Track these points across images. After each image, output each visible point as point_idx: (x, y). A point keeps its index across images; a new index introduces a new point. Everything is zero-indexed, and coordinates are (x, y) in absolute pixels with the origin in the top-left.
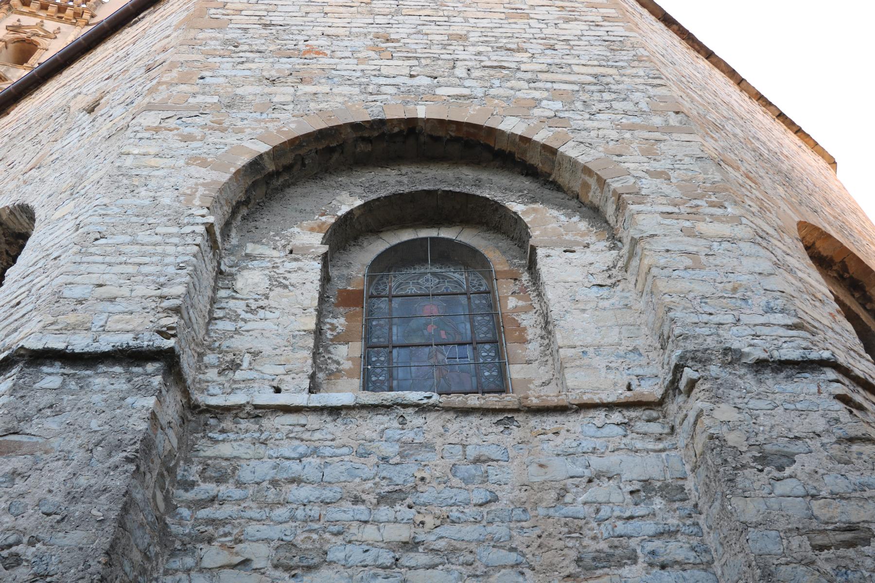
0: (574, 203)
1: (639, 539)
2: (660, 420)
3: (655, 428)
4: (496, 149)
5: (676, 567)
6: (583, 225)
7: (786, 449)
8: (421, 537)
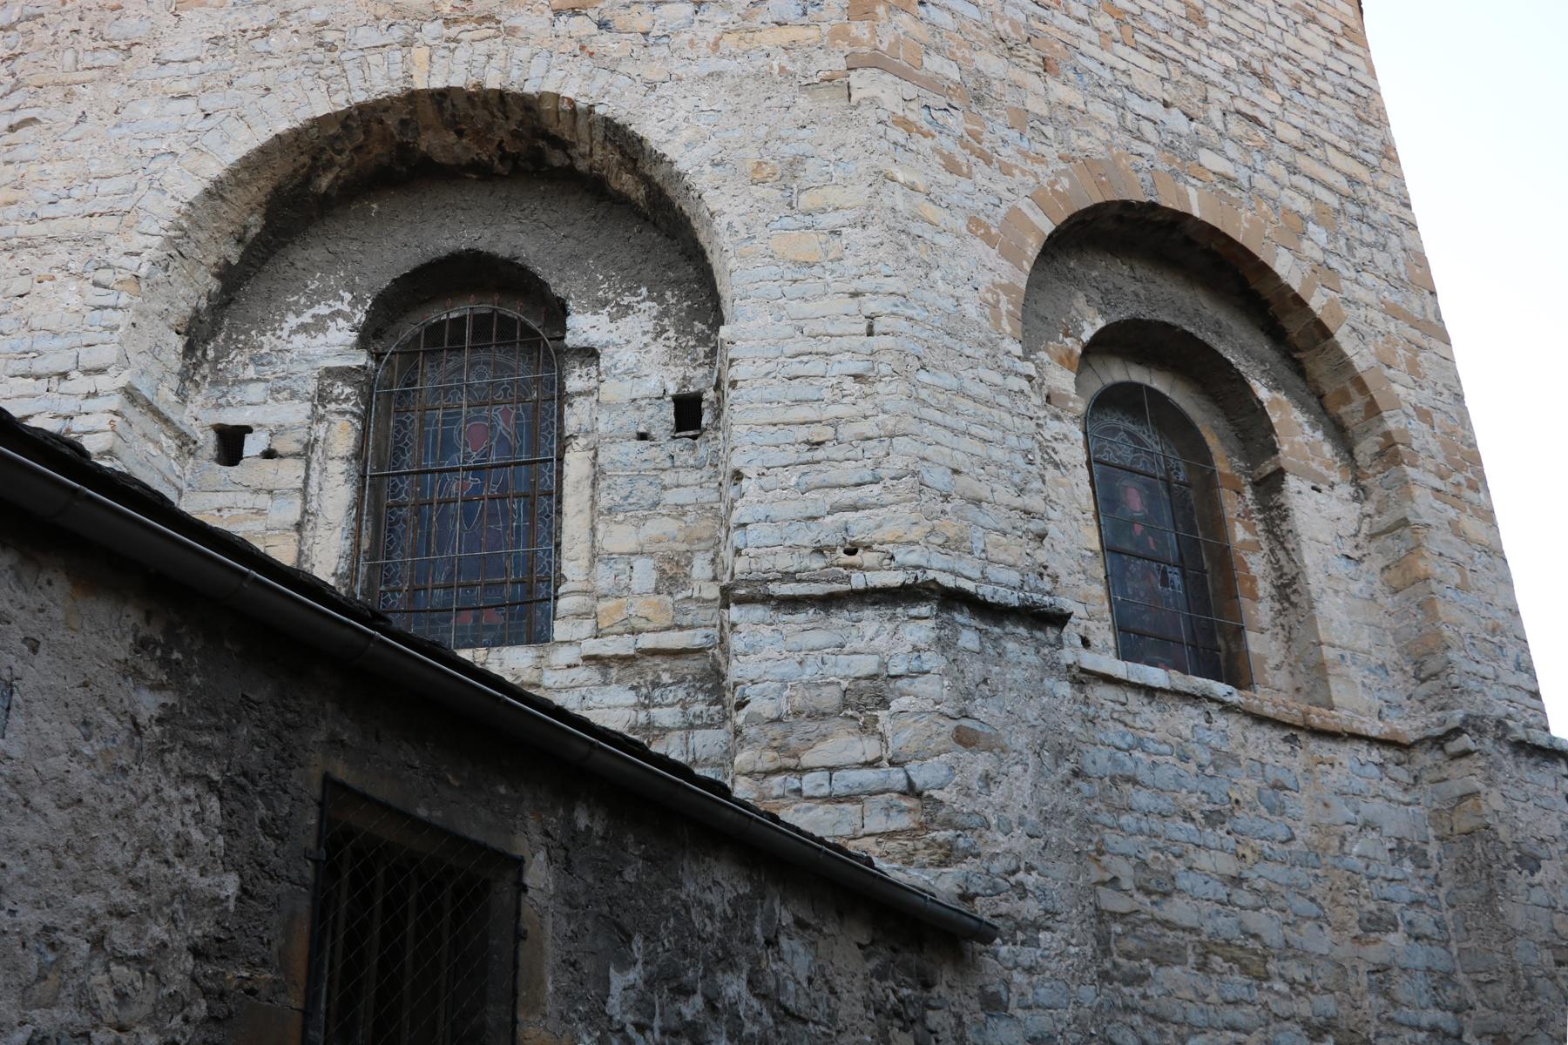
0: (1313, 401)
2: (1406, 766)
3: (1402, 774)
4: (1253, 287)
6: (1327, 449)
8: (1246, 874)
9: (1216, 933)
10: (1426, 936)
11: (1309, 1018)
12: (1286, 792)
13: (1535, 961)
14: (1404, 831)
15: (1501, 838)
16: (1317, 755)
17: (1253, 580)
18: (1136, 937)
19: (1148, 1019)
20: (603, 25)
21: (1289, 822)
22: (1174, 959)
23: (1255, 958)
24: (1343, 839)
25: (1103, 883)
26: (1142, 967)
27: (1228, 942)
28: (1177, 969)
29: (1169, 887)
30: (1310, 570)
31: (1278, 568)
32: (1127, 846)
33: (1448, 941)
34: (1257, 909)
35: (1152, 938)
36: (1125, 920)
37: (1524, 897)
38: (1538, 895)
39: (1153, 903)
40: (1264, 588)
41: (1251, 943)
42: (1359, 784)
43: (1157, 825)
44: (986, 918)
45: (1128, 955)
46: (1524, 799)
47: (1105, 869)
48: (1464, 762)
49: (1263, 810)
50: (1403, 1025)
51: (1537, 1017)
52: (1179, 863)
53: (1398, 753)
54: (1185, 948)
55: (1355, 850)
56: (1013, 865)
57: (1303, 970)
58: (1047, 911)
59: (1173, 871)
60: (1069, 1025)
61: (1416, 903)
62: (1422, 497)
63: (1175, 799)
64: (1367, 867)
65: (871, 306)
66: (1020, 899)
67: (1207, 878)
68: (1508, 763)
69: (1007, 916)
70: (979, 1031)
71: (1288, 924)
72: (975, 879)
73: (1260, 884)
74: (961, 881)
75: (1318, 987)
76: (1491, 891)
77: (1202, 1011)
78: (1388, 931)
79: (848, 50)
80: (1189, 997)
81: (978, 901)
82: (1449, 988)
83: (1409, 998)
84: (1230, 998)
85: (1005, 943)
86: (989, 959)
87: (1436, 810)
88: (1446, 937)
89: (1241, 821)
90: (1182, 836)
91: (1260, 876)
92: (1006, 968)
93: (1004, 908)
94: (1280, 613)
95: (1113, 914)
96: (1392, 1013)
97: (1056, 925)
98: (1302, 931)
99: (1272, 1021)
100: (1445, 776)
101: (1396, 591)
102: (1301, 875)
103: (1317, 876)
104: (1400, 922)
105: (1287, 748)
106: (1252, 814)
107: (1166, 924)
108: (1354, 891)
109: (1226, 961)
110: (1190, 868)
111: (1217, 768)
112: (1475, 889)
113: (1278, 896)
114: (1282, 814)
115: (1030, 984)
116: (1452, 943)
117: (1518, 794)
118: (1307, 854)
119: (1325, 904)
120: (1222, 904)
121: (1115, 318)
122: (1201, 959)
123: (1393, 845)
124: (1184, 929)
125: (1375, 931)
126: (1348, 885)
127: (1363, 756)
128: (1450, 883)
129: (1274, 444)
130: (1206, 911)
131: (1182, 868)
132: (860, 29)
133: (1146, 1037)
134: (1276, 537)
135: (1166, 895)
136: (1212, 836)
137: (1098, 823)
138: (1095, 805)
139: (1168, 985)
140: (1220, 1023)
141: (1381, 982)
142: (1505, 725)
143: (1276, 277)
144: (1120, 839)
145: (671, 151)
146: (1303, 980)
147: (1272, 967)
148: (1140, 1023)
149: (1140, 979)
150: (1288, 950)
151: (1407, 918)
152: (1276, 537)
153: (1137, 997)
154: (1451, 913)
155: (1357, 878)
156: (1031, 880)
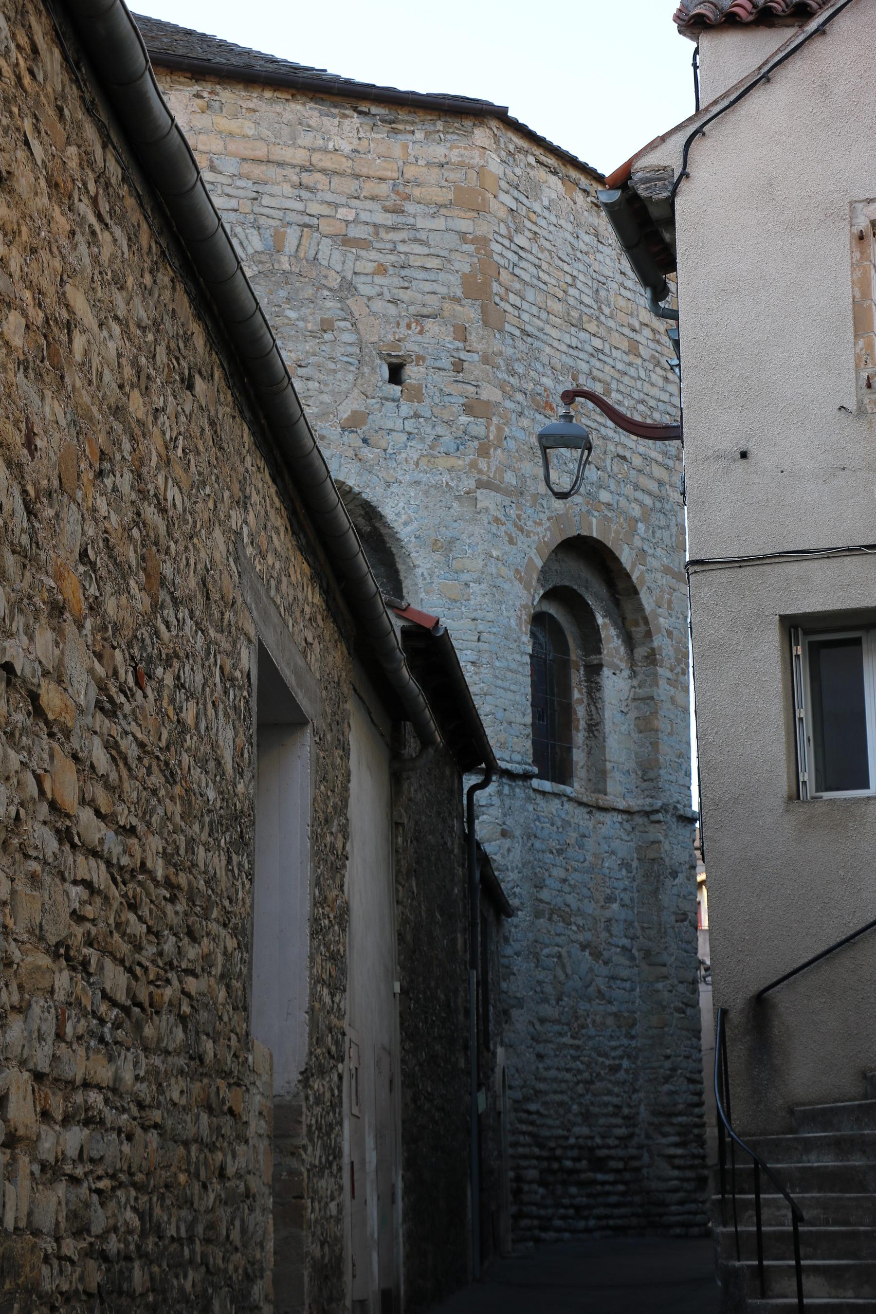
0: (619, 621)
3: (627, 826)
6: (622, 650)
17: (578, 720)
20: (365, 441)
30: (606, 722)
31: (590, 714)
40: (582, 724)
41: (567, 909)
48: (657, 825)
62: (662, 683)
65: (481, 628)
73: (572, 882)
79: (477, 476)
94: (587, 738)
101: (640, 732)
102: (586, 877)
105: (587, 817)
121: (547, 588)
127: (615, 819)
129: (600, 648)
132: (482, 464)
134: (592, 698)
136: (559, 860)
143: (621, 563)
145: (397, 526)
147: (572, 920)
150: (580, 912)
152: (592, 698)
156: (517, 890)
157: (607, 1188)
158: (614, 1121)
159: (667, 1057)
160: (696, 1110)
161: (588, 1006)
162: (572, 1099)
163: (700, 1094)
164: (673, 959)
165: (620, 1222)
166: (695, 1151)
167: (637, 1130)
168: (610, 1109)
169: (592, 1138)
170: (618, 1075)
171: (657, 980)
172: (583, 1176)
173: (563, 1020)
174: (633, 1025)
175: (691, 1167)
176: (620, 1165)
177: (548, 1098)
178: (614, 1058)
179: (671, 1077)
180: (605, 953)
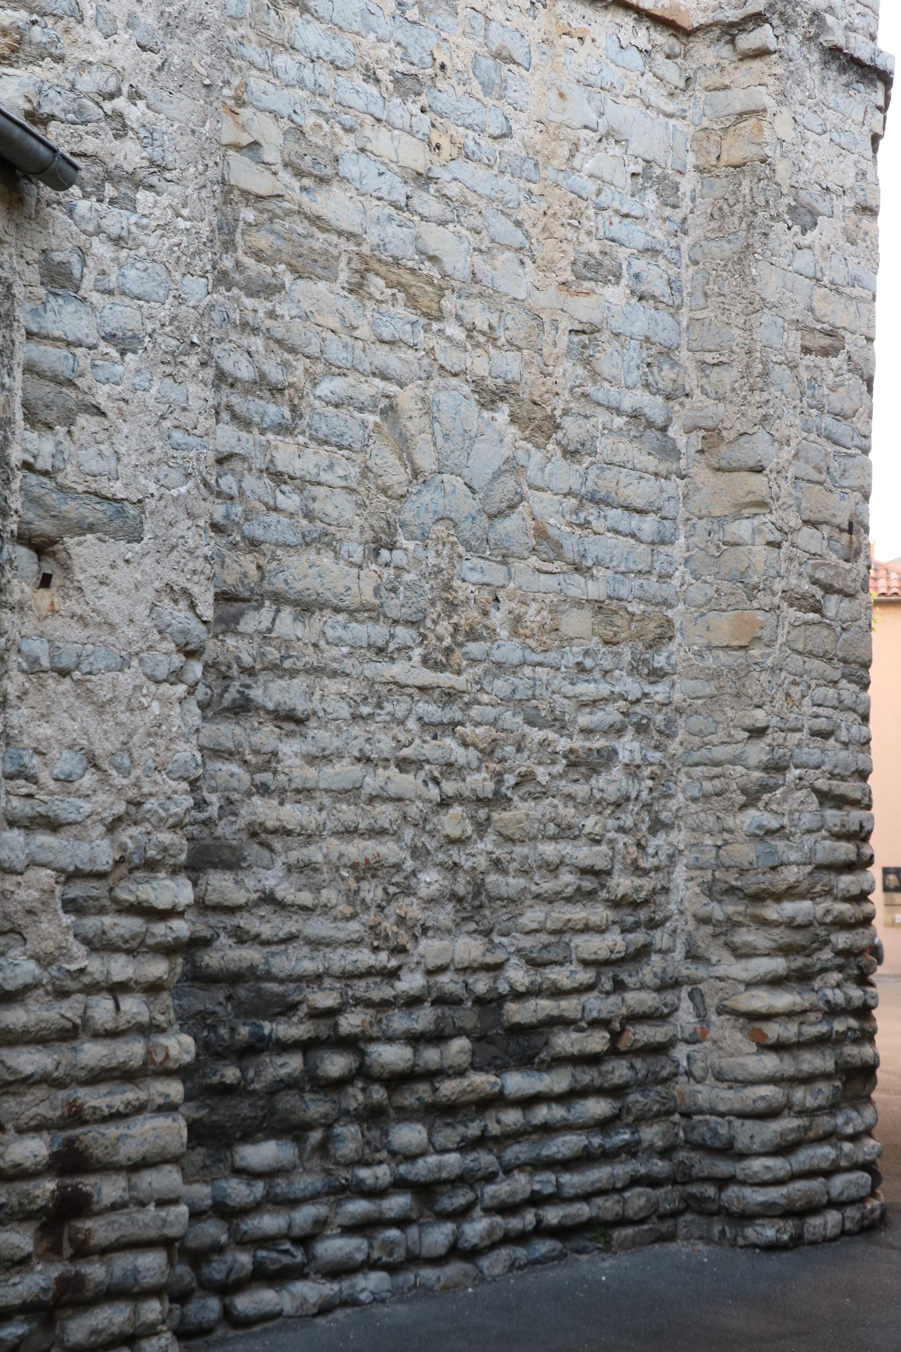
1: (629, 251)
2: (679, 60)
3: (672, 72)
5: (651, 302)
7: (814, 204)
8: (436, 172)
9: (382, 246)
10: (653, 297)
11: (483, 378)
12: (512, 66)
13: (778, 344)
14: (657, 152)
15: (778, 179)
16: (564, 22)
18: (272, 232)
19: (272, 344)
21: (509, 110)
22: (319, 271)
23: (429, 288)
24: (576, 147)
25: (238, 148)
26: (274, 274)
27: (396, 261)
28: (322, 286)
29: (328, 171)
32: (281, 100)
33: (679, 308)
34: (443, 223)
35: (295, 237)
36: (259, 206)
37: (787, 261)
38: (804, 261)
39: (304, 189)
41: (427, 268)
42: (611, 74)
43: (326, 79)
44: (64, 150)
45: (258, 255)
46: (819, 130)
47: (243, 128)
48: (757, 64)
49: (475, 86)
50: (599, 404)
51: (762, 411)
52: (347, 139)
53: (672, 40)
54: (337, 259)
55: (588, 166)
56: (112, 86)
57: (488, 315)
58: (152, 163)
59: (338, 150)
60: (163, 325)
61: (651, 251)
63: (357, 45)
64: (599, 193)
66: (116, 137)
67: (383, 169)
68: (812, 76)
69: (93, 158)
70: (34, 312)
71: (481, 251)
72: (52, 94)
73: (453, 190)
74: (31, 91)
75: (502, 341)
76: (748, 246)
77: (346, 346)
78: (606, 282)
80: (332, 326)
81: (53, 126)
82: (666, 367)
83: (615, 372)
84: (386, 336)
85: (86, 196)
86: (59, 213)
87: (705, 129)
88: (678, 302)
89: (443, 96)
90: (358, 102)
91: (455, 179)
92: (84, 232)
93: (90, 145)
95: (245, 193)
96: (590, 389)
97: (164, 184)
98: (497, 263)
99: (435, 374)
100: (727, 82)
102: (511, 188)
103: (530, 192)
104: (625, 273)
106: (460, 89)
107: (316, 221)
108: (574, 222)
109: (388, 287)
110: (363, 150)
111: (422, 11)
112: (729, 242)
113: (473, 210)
114: (501, 98)
115: (115, 260)
116: (684, 310)
117: (813, 121)
118: (524, 160)
119: (533, 232)
120: (397, 208)
122: (357, 278)
123: (638, 169)
124: (340, 233)
125: (591, 279)
126: (569, 212)
127: (626, 36)
128: (699, 232)
130: (374, 213)
131: (352, 148)
133: (266, 368)
135: (322, 180)
137: (242, 58)
138: (242, 31)
139: (306, 305)
140: (367, 366)
141: (584, 347)
142: (822, 21)
144: (270, 88)
146: (485, 328)
147: (449, 303)
148: (261, 349)
149: (270, 290)
151: (635, 269)
153: (261, 314)
154: (692, 270)
155: (582, 204)
156: (134, 113)
157: (542, 1113)
158: (578, 913)
159: (757, 733)
160: (846, 882)
161: (496, 574)
162: (416, 852)
163: (861, 836)
164: (787, 453)
165: (583, 1211)
166: (837, 997)
167: (660, 938)
168: (567, 878)
169: (497, 968)
170: (599, 781)
171: (738, 511)
172: (449, 1088)
173: (394, 607)
174: (664, 637)
175: (820, 1042)
176: (597, 1041)
177: (314, 853)
178: (587, 732)
179: (766, 788)
180: (568, 422)
